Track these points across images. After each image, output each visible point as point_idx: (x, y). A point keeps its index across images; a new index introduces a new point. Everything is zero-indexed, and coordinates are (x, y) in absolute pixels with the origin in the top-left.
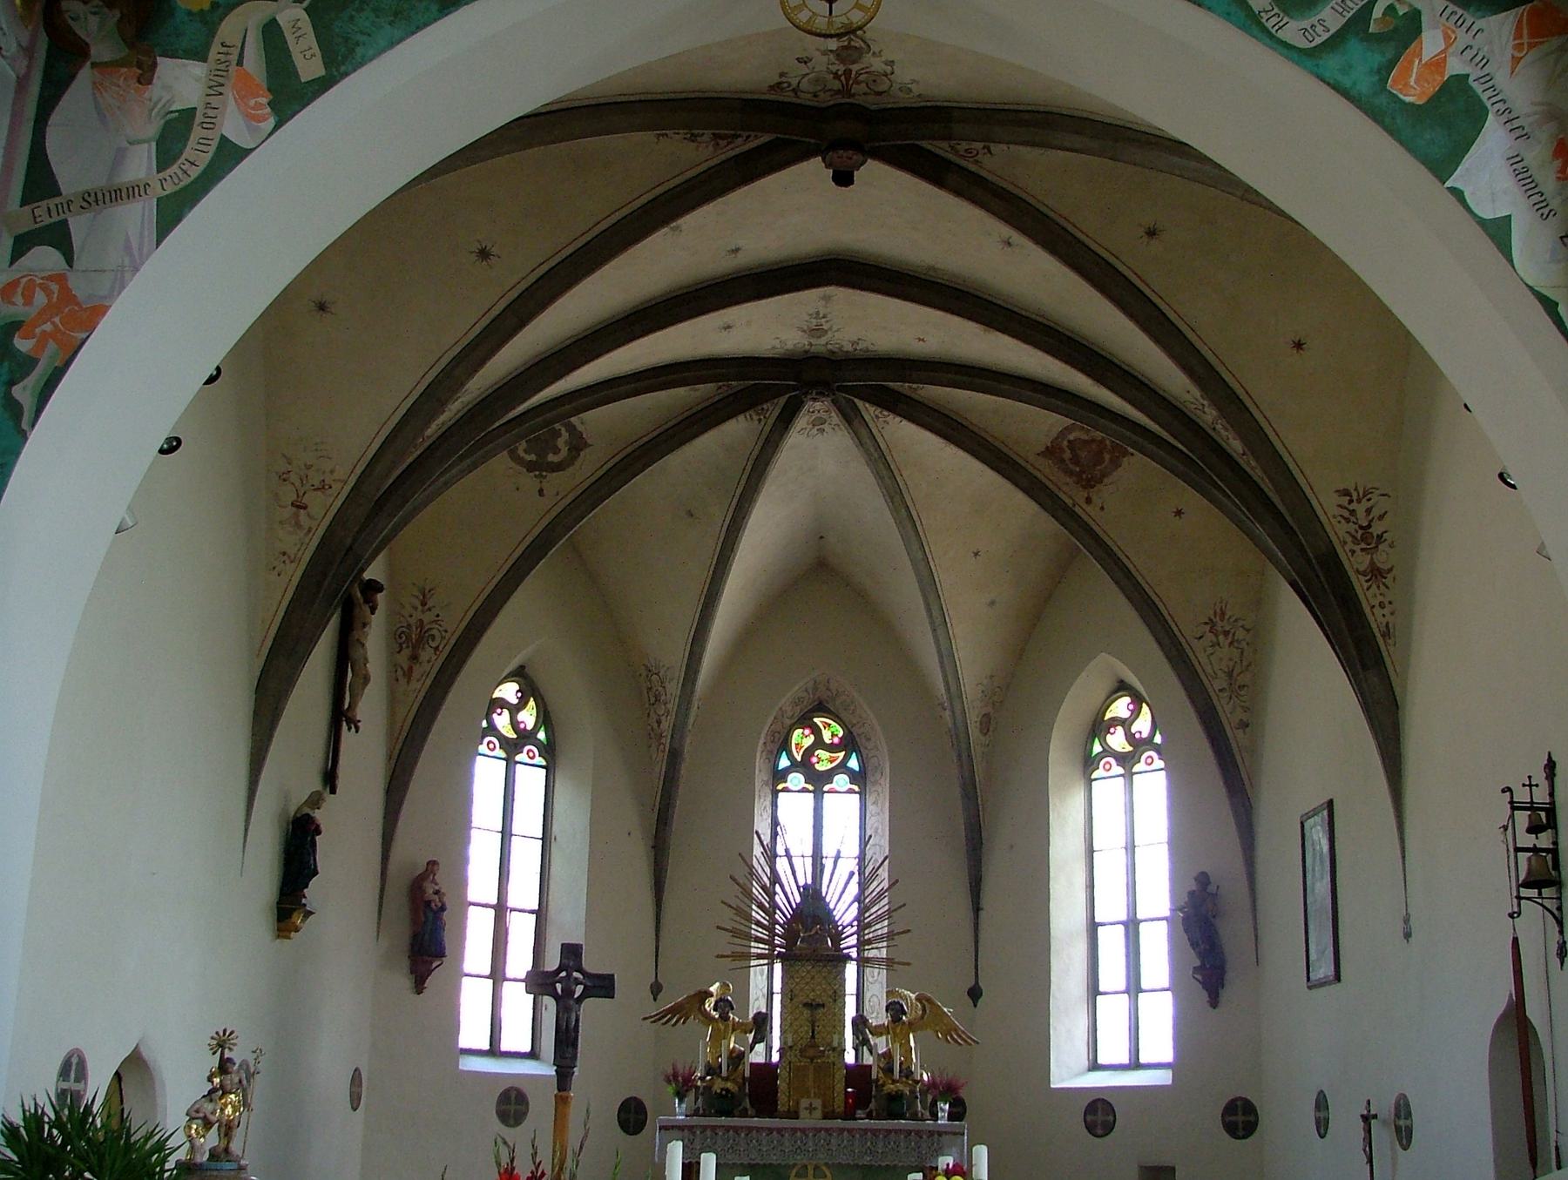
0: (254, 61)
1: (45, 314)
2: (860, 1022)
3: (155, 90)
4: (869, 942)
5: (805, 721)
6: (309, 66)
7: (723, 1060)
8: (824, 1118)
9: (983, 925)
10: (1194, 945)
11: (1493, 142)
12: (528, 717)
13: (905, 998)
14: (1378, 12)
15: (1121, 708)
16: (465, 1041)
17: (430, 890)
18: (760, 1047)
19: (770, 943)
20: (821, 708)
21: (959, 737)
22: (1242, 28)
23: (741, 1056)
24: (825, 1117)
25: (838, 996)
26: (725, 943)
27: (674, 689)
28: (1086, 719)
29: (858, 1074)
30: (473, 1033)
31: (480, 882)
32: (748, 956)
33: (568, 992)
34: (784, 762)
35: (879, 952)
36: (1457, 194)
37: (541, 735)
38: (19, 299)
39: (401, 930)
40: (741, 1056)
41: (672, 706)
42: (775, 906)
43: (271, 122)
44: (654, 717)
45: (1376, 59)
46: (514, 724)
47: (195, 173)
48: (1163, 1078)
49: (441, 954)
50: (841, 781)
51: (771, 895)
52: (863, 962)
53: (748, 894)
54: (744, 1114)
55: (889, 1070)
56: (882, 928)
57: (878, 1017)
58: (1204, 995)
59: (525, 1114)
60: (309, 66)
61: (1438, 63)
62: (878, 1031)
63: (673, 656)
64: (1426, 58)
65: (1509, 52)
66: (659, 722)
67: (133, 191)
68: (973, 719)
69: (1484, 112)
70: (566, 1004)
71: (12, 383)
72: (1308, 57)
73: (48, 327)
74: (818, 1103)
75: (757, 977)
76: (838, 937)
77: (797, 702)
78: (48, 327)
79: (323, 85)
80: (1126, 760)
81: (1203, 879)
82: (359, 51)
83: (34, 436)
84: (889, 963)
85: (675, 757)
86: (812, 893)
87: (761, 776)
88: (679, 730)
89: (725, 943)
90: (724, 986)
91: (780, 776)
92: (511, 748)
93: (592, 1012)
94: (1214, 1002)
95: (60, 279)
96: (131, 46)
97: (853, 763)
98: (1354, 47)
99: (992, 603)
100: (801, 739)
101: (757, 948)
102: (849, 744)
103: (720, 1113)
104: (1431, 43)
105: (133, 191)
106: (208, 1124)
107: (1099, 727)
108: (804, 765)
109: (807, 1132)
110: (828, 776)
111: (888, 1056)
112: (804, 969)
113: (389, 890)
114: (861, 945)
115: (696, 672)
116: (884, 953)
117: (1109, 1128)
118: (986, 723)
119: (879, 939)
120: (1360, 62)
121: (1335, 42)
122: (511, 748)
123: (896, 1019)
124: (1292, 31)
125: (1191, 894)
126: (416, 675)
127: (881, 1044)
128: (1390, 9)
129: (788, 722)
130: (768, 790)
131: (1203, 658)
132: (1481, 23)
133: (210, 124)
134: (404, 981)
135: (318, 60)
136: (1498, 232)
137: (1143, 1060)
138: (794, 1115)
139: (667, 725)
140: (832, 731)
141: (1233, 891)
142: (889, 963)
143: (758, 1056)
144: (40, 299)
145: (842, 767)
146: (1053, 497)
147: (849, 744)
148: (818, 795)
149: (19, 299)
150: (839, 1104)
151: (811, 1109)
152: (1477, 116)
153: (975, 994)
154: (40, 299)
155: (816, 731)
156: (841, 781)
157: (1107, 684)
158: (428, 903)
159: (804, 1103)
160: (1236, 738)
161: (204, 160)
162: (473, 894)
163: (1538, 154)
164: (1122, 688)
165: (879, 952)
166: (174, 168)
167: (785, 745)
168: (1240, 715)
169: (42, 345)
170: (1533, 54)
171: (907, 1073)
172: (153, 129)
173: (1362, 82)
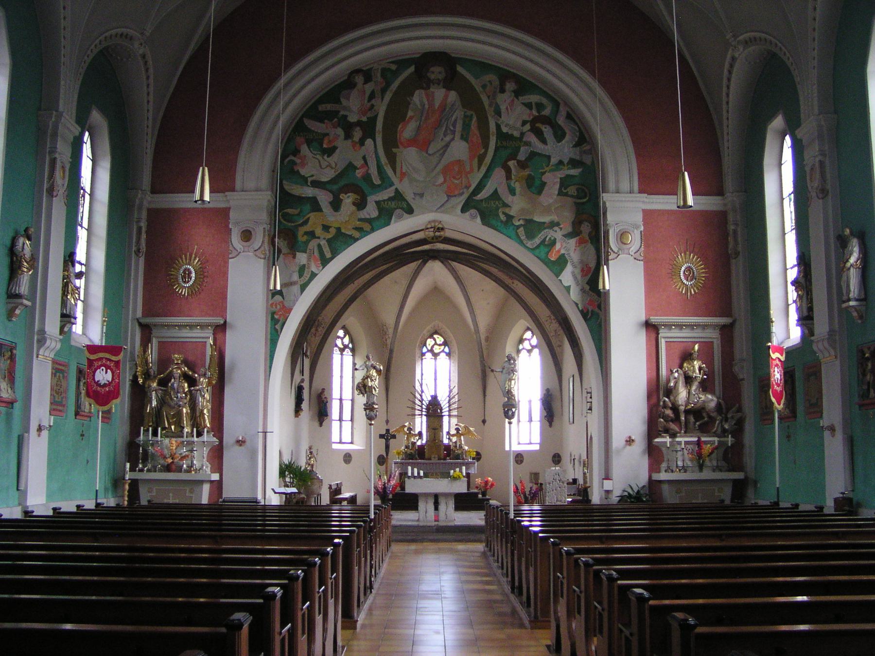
0: (316, 253)
1: (280, 310)
2: (448, 433)
3: (297, 260)
4: (453, 410)
5: (431, 336)
6: (328, 255)
7: (410, 445)
8: (639, 193)
9: (486, 400)
10: (545, 409)
11: (569, 268)
12: (346, 340)
13: (460, 426)
14: (547, 239)
15: (528, 335)
16: (333, 440)
17: (323, 397)
18: (420, 441)
19: (422, 411)
20: (436, 333)
21: (480, 344)
22: (519, 243)
23: (415, 443)
24: (439, 459)
25: (441, 426)
26: (409, 411)
27: (391, 331)
28: (517, 338)
29: (447, 448)
30: (335, 437)
31: (336, 394)
32: (415, 415)
33: (387, 438)
34: (425, 350)
35: (455, 413)
36: (560, 281)
37: (350, 346)
38: (274, 307)
39: (316, 409)
40: (415, 443)
41: (391, 336)
42: (423, 400)
43: (321, 268)
44: (384, 339)
45: (546, 250)
46: (343, 343)
47: (307, 279)
48: (537, 447)
49: (327, 415)
50: (443, 355)
51: (421, 396)
52: (450, 416)
53: (415, 397)
54: (416, 459)
55: (456, 446)
56: (455, 406)
57: (453, 432)
58: (548, 424)
59: (351, 460)
60: (328, 255)
61: (559, 251)
62: (453, 435)
63: (390, 321)
64: (557, 249)
65: (574, 248)
66: (386, 340)
67: (295, 283)
68: (483, 337)
69: (567, 261)
70: (387, 441)
71: (275, 325)
72: (532, 250)
73: (281, 313)
74: (436, 456)
75: (418, 420)
76: (441, 409)
77: (429, 331)
78: (281, 313)
79: (332, 259)
80: (529, 351)
81: (548, 390)
82: (338, 251)
83: (281, 336)
84: (457, 416)
85: (391, 351)
86: (434, 398)
87: (418, 354)
88: (393, 343)
89: (409, 411)
90: (410, 424)
91: (423, 354)
92: (342, 350)
93: (392, 441)
94: (551, 425)
95: (282, 302)
96: (290, 250)
97: (447, 350)
98: (542, 247)
99: (488, 304)
100: (430, 342)
101: (417, 412)
102: (445, 344)
103: (410, 459)
104: (558, 246)
105: (295, 283)
106: (309, 464)
107: (521, 341)
108: (431, 351)
109: (720, 430)
110: (438, 354)
111: (456, 442)
112: (432, 419)
113: (312, 397)
114: (450, 410)
115: (398, 329)
116: (456, 413)
117: (522, 462)
118: (487, 339)
119: (455, 409)
120: (543, 250)
121: (538, 247)
122: (342, 350)
123: (458, 432)
124: (529, 244)
125: (545, 394)
126: (317, 335)
127: (454, 439)
128: (550, 239)
129: (426, 337)
130: (420, 359)
131: (547, 326)
132: (569, 241)
133: (309, 268)
134: (317, 424)
135: (330, 253)
136: (568, 289)
137: (343, 441)
138: (430, 459)
139: (389, 342)
140: (440, 340)
141: (556, 393)
142: (457, 416)
143: (419, 443)
144: (278, 307)
145: (443, 351)
146: (504, 283)
147: (445, 344)
148: (435, 359)
149: (274, 307)
150: (442, 456)
151: (435, 458)
152: (566, 262)
153: (484, 422)
154: (278, 307)
155: (435, 340)
156: (443, 355)
157: (524, 328)
158: (323, 401)
159: (433, 456)
160: (557, 350)
161: (309, 276)
162: (334, 397)
163: (578, 271)
164: (528, 329)
165: (455, 413)
166: (302, 278)
167: (425, 345)
168: (558, 343)
169: (280, 317)
170: (578, 248)
171: (461, 447)
172: (297, 269)
173: (543, 256)
